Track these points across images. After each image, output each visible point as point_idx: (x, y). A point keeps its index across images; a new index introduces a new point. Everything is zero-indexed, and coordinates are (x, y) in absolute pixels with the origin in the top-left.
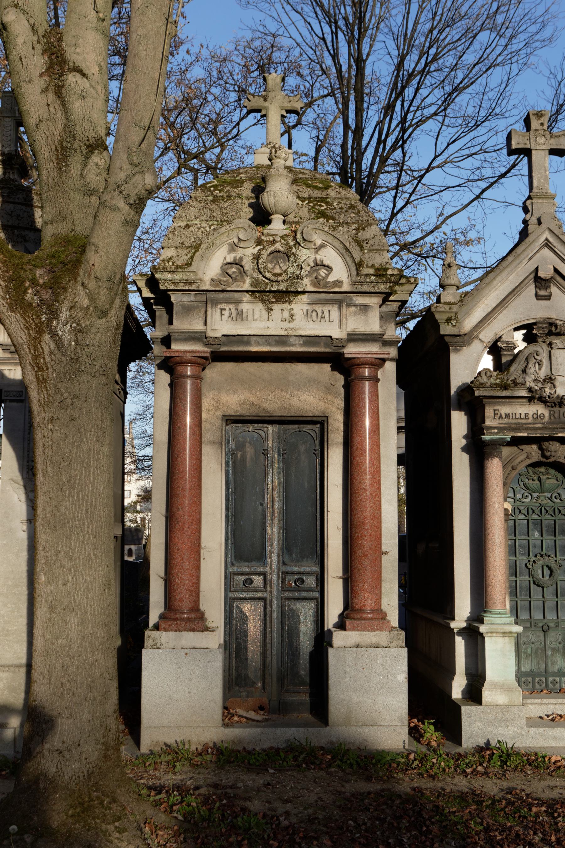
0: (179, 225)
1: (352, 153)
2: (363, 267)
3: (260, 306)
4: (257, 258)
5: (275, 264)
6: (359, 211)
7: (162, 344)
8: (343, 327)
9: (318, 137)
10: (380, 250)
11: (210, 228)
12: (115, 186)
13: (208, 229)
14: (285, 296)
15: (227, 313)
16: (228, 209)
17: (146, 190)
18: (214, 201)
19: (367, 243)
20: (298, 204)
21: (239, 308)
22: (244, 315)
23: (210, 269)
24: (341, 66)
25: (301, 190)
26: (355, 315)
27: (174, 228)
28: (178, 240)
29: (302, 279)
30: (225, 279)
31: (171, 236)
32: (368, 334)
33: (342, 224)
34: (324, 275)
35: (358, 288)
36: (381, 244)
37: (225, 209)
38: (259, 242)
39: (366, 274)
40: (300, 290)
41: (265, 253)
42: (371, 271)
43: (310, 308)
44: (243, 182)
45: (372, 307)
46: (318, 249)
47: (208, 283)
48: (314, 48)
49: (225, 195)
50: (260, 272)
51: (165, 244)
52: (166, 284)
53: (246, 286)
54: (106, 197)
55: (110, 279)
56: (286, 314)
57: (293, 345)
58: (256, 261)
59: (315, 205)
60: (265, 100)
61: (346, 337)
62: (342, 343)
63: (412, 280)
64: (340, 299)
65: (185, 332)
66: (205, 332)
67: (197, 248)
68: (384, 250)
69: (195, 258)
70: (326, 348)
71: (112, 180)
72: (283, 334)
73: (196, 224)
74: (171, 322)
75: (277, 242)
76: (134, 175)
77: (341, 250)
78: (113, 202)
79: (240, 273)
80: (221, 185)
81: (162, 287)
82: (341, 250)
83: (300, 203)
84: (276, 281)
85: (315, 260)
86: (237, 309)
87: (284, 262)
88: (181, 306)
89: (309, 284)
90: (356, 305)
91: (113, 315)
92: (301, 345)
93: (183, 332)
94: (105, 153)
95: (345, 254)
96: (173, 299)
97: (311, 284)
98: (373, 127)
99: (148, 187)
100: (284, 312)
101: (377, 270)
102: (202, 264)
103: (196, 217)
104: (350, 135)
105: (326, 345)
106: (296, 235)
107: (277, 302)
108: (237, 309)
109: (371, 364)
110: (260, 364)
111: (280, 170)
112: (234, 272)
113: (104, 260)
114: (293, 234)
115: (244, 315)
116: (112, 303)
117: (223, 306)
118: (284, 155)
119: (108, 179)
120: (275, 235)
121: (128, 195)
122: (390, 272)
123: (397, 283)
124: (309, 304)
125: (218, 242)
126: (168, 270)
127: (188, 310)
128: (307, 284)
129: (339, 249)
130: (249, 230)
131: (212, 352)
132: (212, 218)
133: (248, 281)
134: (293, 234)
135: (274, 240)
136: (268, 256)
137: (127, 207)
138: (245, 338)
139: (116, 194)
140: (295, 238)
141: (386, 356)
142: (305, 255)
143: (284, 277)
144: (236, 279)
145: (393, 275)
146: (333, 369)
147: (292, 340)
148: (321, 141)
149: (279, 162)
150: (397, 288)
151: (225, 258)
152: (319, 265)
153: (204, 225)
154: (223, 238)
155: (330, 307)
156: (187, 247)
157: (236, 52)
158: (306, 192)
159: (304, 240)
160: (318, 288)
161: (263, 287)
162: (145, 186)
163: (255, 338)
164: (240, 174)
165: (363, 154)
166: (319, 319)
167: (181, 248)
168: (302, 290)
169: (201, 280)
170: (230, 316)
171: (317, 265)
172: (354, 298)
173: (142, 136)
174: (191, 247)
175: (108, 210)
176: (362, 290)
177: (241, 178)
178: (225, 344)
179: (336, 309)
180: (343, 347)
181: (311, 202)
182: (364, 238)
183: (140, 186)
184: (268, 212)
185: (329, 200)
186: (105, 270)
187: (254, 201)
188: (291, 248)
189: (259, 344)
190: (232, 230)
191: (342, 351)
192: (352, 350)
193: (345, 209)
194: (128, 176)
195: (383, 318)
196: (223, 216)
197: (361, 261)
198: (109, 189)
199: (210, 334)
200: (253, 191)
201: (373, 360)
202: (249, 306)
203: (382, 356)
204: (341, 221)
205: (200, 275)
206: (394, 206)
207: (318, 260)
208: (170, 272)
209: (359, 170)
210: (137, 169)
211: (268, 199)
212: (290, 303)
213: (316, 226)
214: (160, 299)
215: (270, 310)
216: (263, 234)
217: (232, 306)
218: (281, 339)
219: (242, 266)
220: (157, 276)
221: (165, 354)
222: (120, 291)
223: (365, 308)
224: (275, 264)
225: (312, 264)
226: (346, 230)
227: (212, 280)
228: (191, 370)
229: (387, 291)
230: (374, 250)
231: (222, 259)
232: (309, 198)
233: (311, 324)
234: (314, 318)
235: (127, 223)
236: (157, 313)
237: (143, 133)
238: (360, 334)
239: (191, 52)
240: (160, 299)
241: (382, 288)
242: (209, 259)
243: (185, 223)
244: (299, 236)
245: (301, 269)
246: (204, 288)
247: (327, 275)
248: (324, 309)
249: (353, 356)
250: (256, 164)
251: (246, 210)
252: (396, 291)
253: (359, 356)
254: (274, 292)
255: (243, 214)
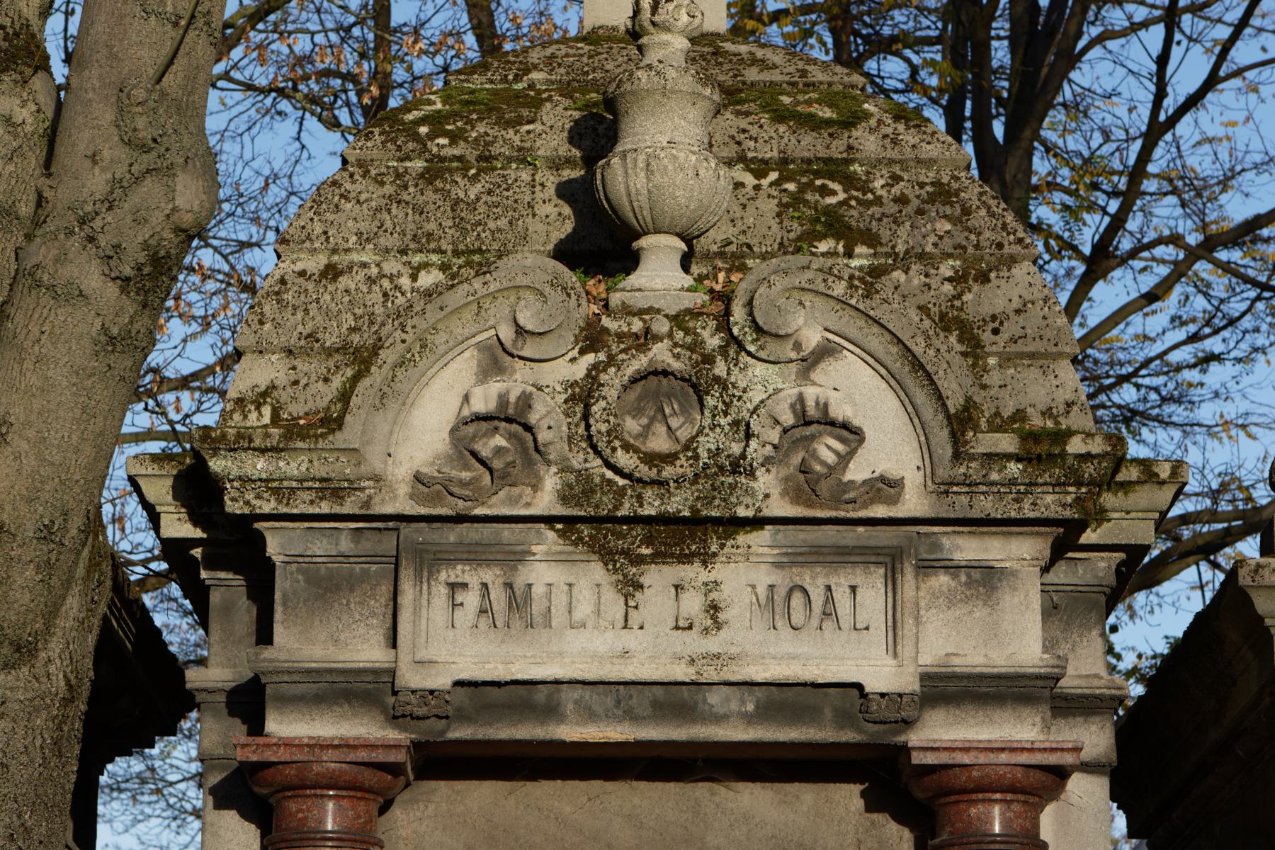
0: (299, 266)
2: (976, 429)
3: (596, 571)
4: (582, 396)
5: (652, 420)
6: (966, 211)
8: (907, 650)
10: (1046, 355)
11: (414, 278)
12: (71, 217)
13: (405, 281)
14: (691, 535)
15: (471, 599)
16: (482, 208)
17: (178, 230)
18: (430, 176)
19: (996, 332)
20: (739, 185)
21: (519, 583)
23: (415, 434)
25: (754, 130)
26: (951, 604)
27: (283, 281)
28: (295, 326)
29: (751, 474)
30: (466, 475)
32: (999, 677)
33: (902, 262)
34: (830, 458)
35: (961, 505)
36: (1049, 334)
37: (472, 206)
38: (592, 338)
40: (742, 512)
41: (613, 381)
42: (1006, 443)
43: (782, 579)
44: (537, 103)
45: (1014, 573)
46: (811, 361)
47: (403, 490)
50: (594, 447)
51: (246, 339)
52: (250, 496)
53: (546, 501)
54: (41, 253)
55: (47, 534)
56: (693, 604)
57: (718, 719)
58: (579, 409)
59: (802, 189)
62: (900, 711)
63: (1164, 471)
64: (895, 548)
65: (318, 671)
66: (392, 672)
68: (1059, 356)
69: (354, 401)
70: (841, 727)
71: (61, 196)
72: (680, 677)
73: (364, 265)
74: (264, 635)
75: (657, 338)
76: (137, 180)
77: (896, 366)
78: (66, 272)
79: (525, 450)
80: (455, 115)
81: (232, 507)
83: (749, 180)
84: (653, 482)
85: (799, 405)
86: (509, 586)
87: (685, 411)
88: (305, 573)
89: (775, 492)
90: (952, 568)
91: (54, 655)
92: (750, 719)
93: (309, 671)
94: (38, 82)
95: (909, 381)
96: (273, 547)
97: (784, 493)
99: (187, 219)
100: (684, 596)
102: (381, 423)
103: (364, 240)
105: (843, 718)
106: (728, 313)
108: (509, 586)
110: (596, 785)
111: (671, 74)
112: (499, 451)
113: (27, 469)
114: (718, 307)
115: (537, 608)
116: (52, 612)
117: (459, 573)
118: (685, 18)
119: (47, 194)
120: (650, 310)
121: (117, 247)
122: (1076, 446)
123: (1109, 482)
124: (778, 565)
125: (441, 338)
126: (257, 442)
127: (329, 587)
130: (556, 296)
131: (416, 746)
132: (424, 241)
133: (551, 482)
134: (718, 307)
135: (647, 331)
136: (625, 388)
137: (112, 290)
138: (541, 694)
139: (75, 244)
140: (724, 323)
141: (1068, 759)
142: (763, 383)
143: (682, 467)
145: (1088, 457)
146: (873, 803)
147: (714, 698)
149: (666, 44)
150: (1108, 499)
151: (466, 398)
152: (813, 421)
153: (391, 266)
154: (460, 328)
155: (858, 578)
156: (329, 352)
158: (772, 140)
159: (758, 329)
160: (809, 504)
162: (175, 218)
163: (577, 692)
164: (527, 71)
166: (815, 622)
167: (307, 353)
168: (750, 513)
169: (377, 479)
170: (483, 611)
171: (808, 423)
172: (946, 541)
173: (167, 50)
174: (343, 349)
175: (46, 299)
176: (975, 514)
177: (531, 86)
178: (463, 716)
180: (907, 724)
181: (789, 180)
182: (986, 310)
183: (157, 218)
184: (625, 224)
185: (856, 168)
186: (30, 501)
187: (577, 173)
188: (709, 360)
189: (590, 715)
191: (901, 739)
192: (941, 734)
193: (915, 203)
194: (115, 182)
197: (969, 405)
198: (50, 227)
199: (411, 678)
200: (575, 136)
201: (1019, 773)
202: (549, 570)
203: (1053, 759)
204: (901, 248)
205: (375, 461)
206: (1160, 95)
207: (810, 403)
208: (263, 451)
210: (148, 160)
211: (625, 180)
212: (707, 559)
213: (802, 279)
214: (225, 547)
216: (606, 306)
217: (490, 575)
218: (675, 698)
219: (528, 428)
220: (216, 465)
221: (240, 755)
222: (80, 571)
223: (986, 579)
224: (652, 420)
225: (788, 419)
226: (917, 280)
228: (339, 810)
229: (1067, 513)
230: (1022, 355)
231: (455, 402)
232: (783, 162)
233: (785, 642)
234: (798, 616)
235: (111, 342)
236: (215, 597)
237: (173, 33)
238: (969, 677)
240: (225, 547)
241: (1050, 503)
242: (406, 402)
243: (322, 260)
245: (749, 436)
246: (389, 509)
247: (844, 460)
248: (832, 581)
249: (944, 758)
251: (549, 209)
252: (1103, 511)
253: (966, 759)
254: (648, 520)
255: (534, 226)
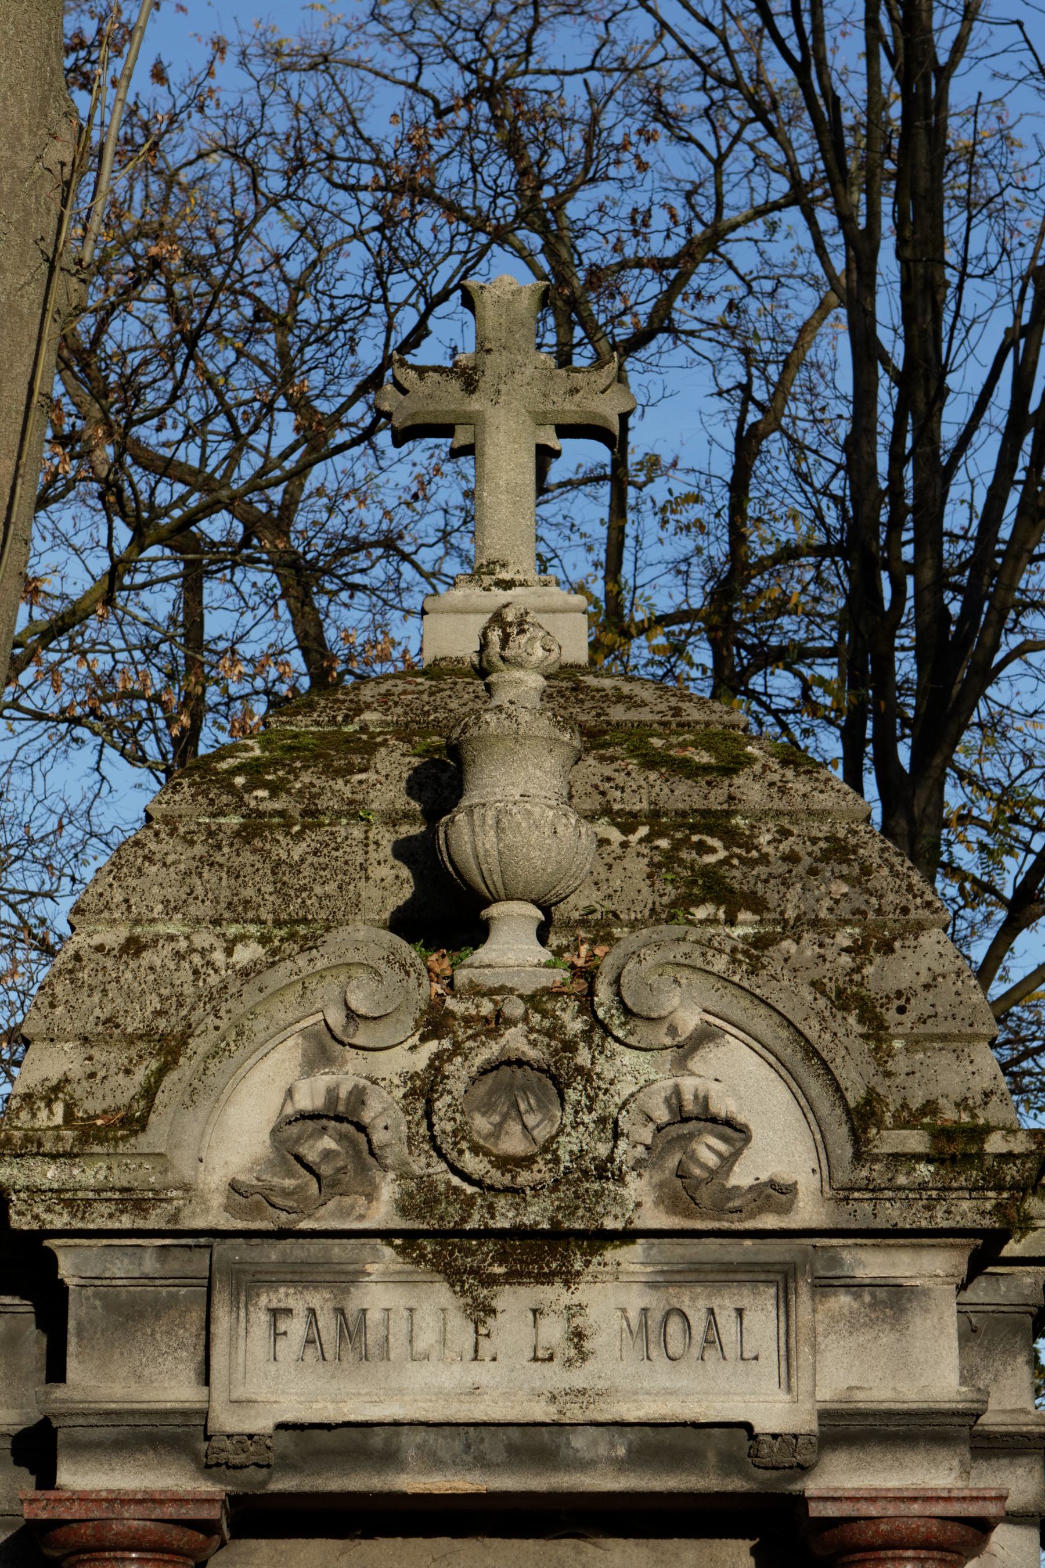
0: (97, 940)
1: (895, 476)
2: (880, 1125)
3: (441, 1294)
4: (425, 1089)
5: (505, 1117)
6: (866, 871)
7: (18, 1462)
8: (802, 1382)
9: (746, 389)
10: (959, 1037)
11: (229, 952)
14: (549, 1252)
15: (296, 1327)
16: (307, 870)
18: (247, 834)
19: (901, 1010)
20: (603, 842)
22: (372, 1337)
23: (230, 1136)
24: (834, 103)
25: (620, 778)
26: (853, 1329)
27: (77, 957)
28: (93, 1008)
29: (620, 1179)
30: (289, 1183)
31: (60, 989)
33: (794, 929)
34: (711, 1160)
35: (863, 1213)
36: (963, 1012)
37: (296, 868)
38: (435, 1022)
39: (896, 1156)
40: (609, 1224)
41: (459, 1073)
42: (916, 1141)
43: (656, 1301)
44: (370, 748)
45: (926, 1292)
47: (217, 1201)
48: (716, 22)
49: (295, 809)
50: (438, 1149)
52: (39, 1209)
53: (382, 1212)
56: (553, 1332)
57: (584, 1465)
58: (420, 1105)
60: (470, 385)
61: (814, 1426)
62: (797, 1454)
65: (118, 1413)
66: (205, 1414)
67: (170, 1049)
68: (976, 1037)
69: (160, 1098)
72: (540, 1417)
73: (171, 938)
75: (510, 1023)
77: (786, 1053)
80: (274, 764)
82: (786, 1053)
83: (615, 836)
86: (340, 1311)
88: (103, 1297)
89: (648, 1201)
90: (854, 1287)
92: (621, 1466)
93: (108, 1413)
96: (67, 1269)
97: (659, 1202)
98: (989, 361)
100: (543, 1322)
101: (942, 1134)
103: (171, 908)
104: (886, 395)
105: (729, 1463)
106: (591, 992)
107: (513, 1277)
108: (340, 1311)
109: (927, 1545)
111: (525, 717)
112: (328, 1155)
117: (282, 1296)
118: (540, 653)
120: (502, 990)
122: (995, 1144)
124: (652, 1285)
125: (260, 1024)
126: (48, 1147)
127: (131, 1314)
128: (640, 1200)
129: (778, 1048)
130: (392, 975)
131: (233, 1499)
132: (240, 909)
133: (388, 1190)
135: (499, 1013)
136: (473, 1080)
140: (587, 1004)
141: (991, 1509)
143: (541, 1172)
144: (335, 1184)
147: (579, 1441)
148: (759, 405)
149: (518, 682)
151: (290, 1093)
152: (692, 1117)
153: (203, 939)
154: (283, 1011)
156: (131, 1040)
157: (374, 28)
158: (640, 789)
160: (688, 1214)
161: (451, 1215)
163: (420, 1436)
164: (359, 711)
165: (948, 473)
166: (695, 1351)
167: (105, 1040)
168: (619, 1225)
169: (186, 1188)
170: (309, 1341)
171: (685, 1120)
172: (846, 1256)
176: (880, 1224)
177: (364, 729)
178: (287, 1465)
179: (770, 1305)
180: (804, 1469)
181: (661, 835)
182: (890, 985)
185: (738, 821)
187: (416, 830)
188: (570, 1047)
189: (435, 1462)
190: (321, 975)
191: (797, 1487)
193: (807, 861)
195: (977, 1333)
196: (287, 899)
197: (872, 1098)
199: (227, 1420)
200: (415, 786)
201: (935, 1527)
203: (973, 1510)
204: (791, 914)
205: (184, 1167)
207: (688, 1097)
208: (54, 1157)
209: (931, 531)
211: (473, 839)
212: (570, 1279)
213: (677, 952)
215: (481, 1312)
216: (451, 985)
217: (317, 1299)
218: (533, 1441)
219: (362, 1128)
221: (28, 1512)
223: (893, 1299)
224: (505, 1117)
225: (662, 1115)
226: (811, 951)
227: (234, 1187)
229: (987, 1223)
231: (277, 1098)
232: (654, 814)
233: (661, 1374)
234: (676, 1345)
238: (875, 1414)
239: (171, 74)
241: (967, 1211)
242: (220, 1099)
243: (123, 932)
244: (604, 993)
245: (617, 1135)
246: (200, 1223)
247: (728, 1162)
248: (716, 1303)
250: (428, 657)
251: (384, 871)
252: (1028, 1218)
253: (873, 1511)
255: (369, 891)
